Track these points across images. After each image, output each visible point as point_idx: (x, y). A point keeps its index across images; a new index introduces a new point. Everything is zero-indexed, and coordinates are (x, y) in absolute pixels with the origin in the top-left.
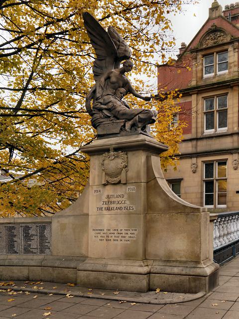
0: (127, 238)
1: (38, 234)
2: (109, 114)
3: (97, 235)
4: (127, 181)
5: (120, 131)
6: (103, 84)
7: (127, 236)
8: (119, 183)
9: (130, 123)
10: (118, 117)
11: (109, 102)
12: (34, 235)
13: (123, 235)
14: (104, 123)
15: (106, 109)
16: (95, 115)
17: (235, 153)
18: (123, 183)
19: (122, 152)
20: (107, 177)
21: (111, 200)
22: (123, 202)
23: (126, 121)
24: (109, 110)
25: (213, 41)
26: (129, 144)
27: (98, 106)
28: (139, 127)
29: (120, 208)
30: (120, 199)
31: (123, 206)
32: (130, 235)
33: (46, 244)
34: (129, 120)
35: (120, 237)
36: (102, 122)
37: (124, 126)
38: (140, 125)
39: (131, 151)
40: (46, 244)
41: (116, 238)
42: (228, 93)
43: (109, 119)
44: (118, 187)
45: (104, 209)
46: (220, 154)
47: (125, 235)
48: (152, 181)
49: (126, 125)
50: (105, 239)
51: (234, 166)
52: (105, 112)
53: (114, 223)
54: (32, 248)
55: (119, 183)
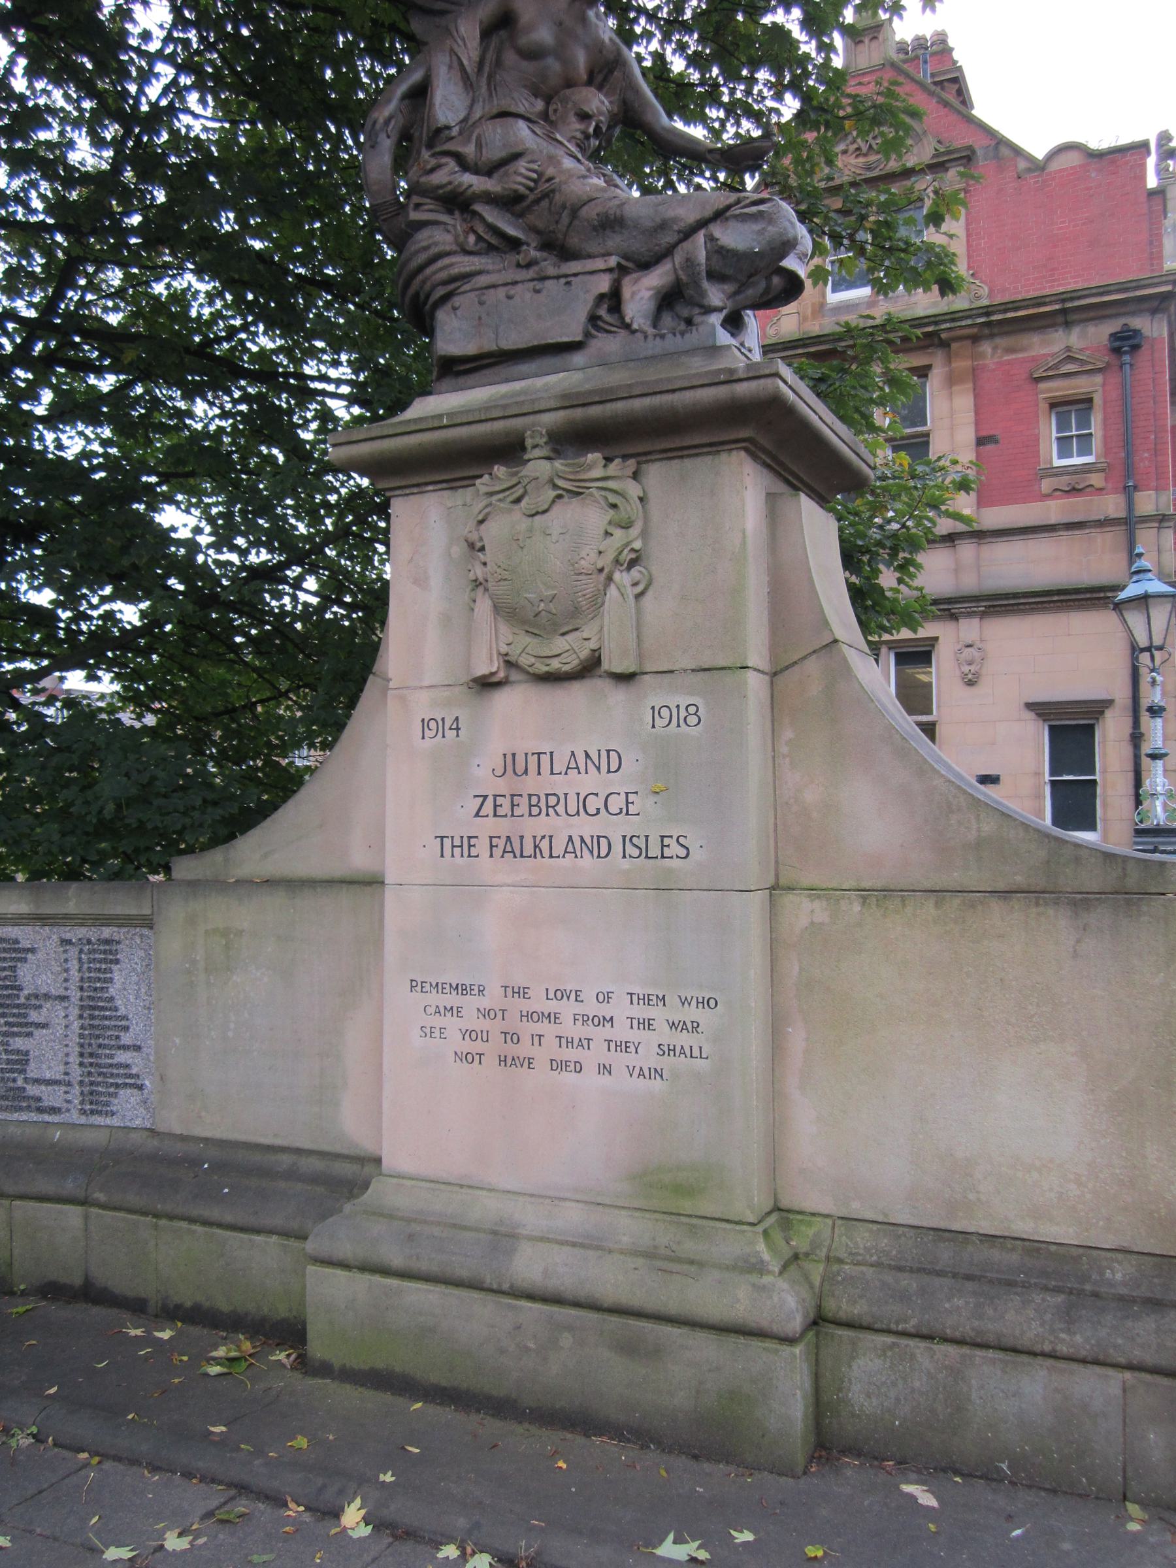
0: (648, 1058)
1: (75, 994)
2: (516, 227)
3: (438, 1022)
4: (640, 656)
5: (587, 335)
6: (475, 55)
7: (649, 1040)
8: (590, 667)
9: (656, 279)
10: (574, 241)
11: (516, 156)
12: (47, 996)
13: (620, 1031)
14: (482, 280)
15: (490, 199)
16: (423, 237)
17: (970, 615)
18: (618, 669)
19: (608, 460)
20: (505, 631)
21: (531, 784)
22: (616, 803)
23: (622, 270)
24: (511, 202)
25: (861, 160)
26: (638, 404)
27: (439, 178)
28: (709, 310)
29: (596, 846)
30: (589, 782)
31: (616, 829)
32: (663, 1034)
33: (122, 1057)
34: (645, 265)
35: (598, 1046)
36: (466, 277)
37: (614, 300)
38: (715, 295)
39: (670, 454)
40: (122, 1057)
41: (571, 1054)
42: (929, 367)
43: (512, 258)
44: (577, 694)
45: (482, 847)
47: (634, 1035)
48: (813, 667)
49: (626, 292)
50: (493, 1048)
51: (966, 669)
52: (491, 215)
54: (37, 1081)
55: (590, 667)
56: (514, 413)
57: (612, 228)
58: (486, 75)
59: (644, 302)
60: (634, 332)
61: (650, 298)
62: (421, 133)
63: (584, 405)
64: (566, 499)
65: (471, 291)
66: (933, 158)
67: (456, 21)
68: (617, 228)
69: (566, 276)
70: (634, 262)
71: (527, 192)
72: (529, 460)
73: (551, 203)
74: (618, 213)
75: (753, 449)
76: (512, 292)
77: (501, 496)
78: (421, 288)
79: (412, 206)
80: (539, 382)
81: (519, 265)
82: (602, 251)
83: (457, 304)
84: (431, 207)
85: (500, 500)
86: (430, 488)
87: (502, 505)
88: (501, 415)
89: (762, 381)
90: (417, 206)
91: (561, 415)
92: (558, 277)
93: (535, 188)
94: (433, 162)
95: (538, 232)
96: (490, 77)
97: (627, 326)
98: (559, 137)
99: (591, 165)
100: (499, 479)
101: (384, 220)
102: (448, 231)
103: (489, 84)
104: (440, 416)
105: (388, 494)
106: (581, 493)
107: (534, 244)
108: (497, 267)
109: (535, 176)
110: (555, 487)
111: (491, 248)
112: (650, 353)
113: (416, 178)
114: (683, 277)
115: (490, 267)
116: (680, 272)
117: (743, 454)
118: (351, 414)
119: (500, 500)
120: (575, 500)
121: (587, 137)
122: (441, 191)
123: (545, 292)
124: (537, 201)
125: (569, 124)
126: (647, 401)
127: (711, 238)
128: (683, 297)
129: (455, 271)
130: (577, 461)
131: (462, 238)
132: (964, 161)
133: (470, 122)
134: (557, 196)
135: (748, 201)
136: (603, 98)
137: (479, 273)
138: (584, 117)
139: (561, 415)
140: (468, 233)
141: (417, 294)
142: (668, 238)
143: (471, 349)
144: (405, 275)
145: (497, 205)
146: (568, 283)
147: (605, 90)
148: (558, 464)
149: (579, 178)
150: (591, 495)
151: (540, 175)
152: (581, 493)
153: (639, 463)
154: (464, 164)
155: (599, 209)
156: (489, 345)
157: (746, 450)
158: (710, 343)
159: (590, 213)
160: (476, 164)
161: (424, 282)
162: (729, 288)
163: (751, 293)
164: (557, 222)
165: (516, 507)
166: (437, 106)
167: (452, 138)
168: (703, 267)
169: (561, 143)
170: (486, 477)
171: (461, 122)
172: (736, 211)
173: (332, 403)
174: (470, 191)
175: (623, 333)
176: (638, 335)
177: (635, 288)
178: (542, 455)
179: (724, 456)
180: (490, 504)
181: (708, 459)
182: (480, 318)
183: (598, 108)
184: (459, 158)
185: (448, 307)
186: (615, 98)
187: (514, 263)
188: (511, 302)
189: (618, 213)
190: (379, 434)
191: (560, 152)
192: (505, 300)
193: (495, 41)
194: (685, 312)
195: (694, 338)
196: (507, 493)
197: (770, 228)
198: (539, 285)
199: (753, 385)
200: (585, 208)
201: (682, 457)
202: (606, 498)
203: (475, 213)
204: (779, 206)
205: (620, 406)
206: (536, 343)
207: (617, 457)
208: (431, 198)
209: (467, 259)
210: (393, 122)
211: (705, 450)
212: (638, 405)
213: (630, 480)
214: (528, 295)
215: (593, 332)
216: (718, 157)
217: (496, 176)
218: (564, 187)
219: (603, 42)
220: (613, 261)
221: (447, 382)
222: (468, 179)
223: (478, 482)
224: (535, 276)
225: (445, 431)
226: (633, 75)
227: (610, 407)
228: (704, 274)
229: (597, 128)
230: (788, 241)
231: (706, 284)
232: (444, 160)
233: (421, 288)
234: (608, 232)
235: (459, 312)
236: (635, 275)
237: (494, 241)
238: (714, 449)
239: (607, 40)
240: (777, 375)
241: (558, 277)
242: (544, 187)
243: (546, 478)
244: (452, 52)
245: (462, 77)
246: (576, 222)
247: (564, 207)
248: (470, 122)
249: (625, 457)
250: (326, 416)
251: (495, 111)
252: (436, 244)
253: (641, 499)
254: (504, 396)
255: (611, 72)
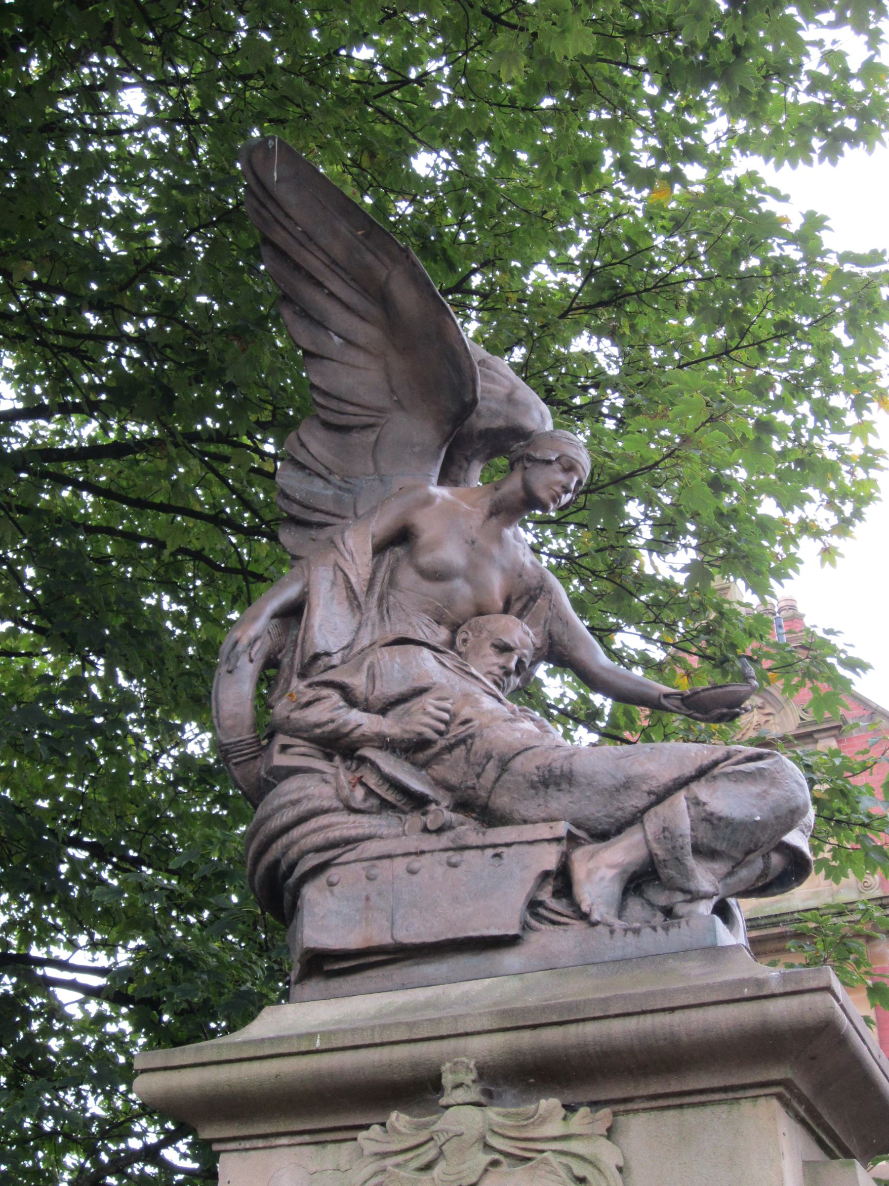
2: (421, 780)
5: (526, 926)
10: (502, 801)
11: (420, 692)
14: (372, 848)
16: (290, 788)
19: (570, 1108)
23: (572, 840)
27: (314, 715)
28: (695, 897)
34: (602, 836)
43: (414, 820)
46: (828, 1146)
53: (38, 1022)
56: (426, 1035)
57: (558, 785)
58: (376, 596)
59: (605, 883)
60: (594, 924)
61: (612, 879)
62: (293, 659)
63: (534, 1027)
64: (504, 1168)
65: (355, 861)
66: (799, 727)
67: (343, 533)
68: (564, 786)
69: (495, 846)
70: (587, 830)
71: (435, 736)
72: (447, 1107)
73: (469, 751)
74: (566, 768)
75: (788, 1096)
76: (416, 865)
77: (400, 1158)
78: (284, 854)
79: (277, 748)
80: (455, 991)
81: (425, 830)
82: (543, 815)
83: (334, 879)
84: (303, 750)
85: (398, 1165)
86: (284, 1141)
87: (402, 1173)
88: (405, 1037)
89: (806, 998)
90: (284, 748)
91: (499, 1041)
92: (483, 847)
93: (447, 732)
94: (310, 694)
95: (449, 788)
96: (381, 599)
97: (584, 917)
98: (474, 671)
99: (515, 706)
100: (398, 1132)
101: (236, 764)
102: (326, 782)
103: (380, 605)
104: (311, 1036)
105: (216, 1147)
106: (529, 1159)
107: (445, 803)
108: (393, 831)
109: (446, 716)
110: (488, 1147)
111: (385, 805)
112: (619, 954)
113: (286, 714)
114: (660, 853)
115: (385, 831)
116: (654, 846)
117: (775, 1103)
118: (86, 1013)
119: (398, 1165)
120: (520, 1169)
121: (507, 673)
122: (318, 731)
123: (463, 867)
124: (450, 748)
125: (484, 656)
126: (632, 1024)
127: (696, 802)
128: (658, 878)
129: (335, 834)
130: (521, 1109)
131: (346, 792)
132: (835, 732)
133: (357, 648)
134: (478, 742)
135: (741, 756)
136: (527, 628)
137: (369, 838)
138: (504, 649)
139: (499, 1041)
140: (354, 786)
141: (277, 863)
142: (638, 801)
143: (352, 940)
144: (260, 837)
145: (394, 751)
146: (497, 855)
147: (526, 619)
148: (493, 1114)
149: (505, 721)
150: (546, 1162)
151: (454, 716)
152: (529, 1159)
153: (615, 1114)
154: (351, 701)
155: (539, 761)
156: (381, 937)
157: (779, 1097)
158: (708, 942)
159: (523, 765)
160: (366, 700)
161: (288, 847)
162: (721, 867)
163: (747, 874)
164: (478, 776)
165: (425, 1177)
166: (316, 628)
167: (333, 667)
168: (688, 840)
169: (477, 678)
170: (376, 1128)
171: (344, 648)
172: (727, 768)
173: (63, 995)
174: (358, 733)
175: (578, 926)
176: (600, 928)
177: (591, 865)
178: (468, 1099)
179: (746, 1107)
180: (384, 1171)
181: (721, 1111)
182: (367, 899)
183: (520, 640)
184: (343, 690)
185: (322, 880)
186: (540, 629)
187: (420, 825)
188: (415, 878)
189: (566, 768)
190: (215, 1058)
191: (475, 689)
192: (405, 875)
193: (388, 558)
194: (662, 899)
195: (680, 935)
196: (410, 1155)
197: (773, 791)
198: (455, 857)
199: (794, 1003)
200: (520, 759)
201: (681, 1106)
202: (569, 1169)
203: (363, 760)
204: (783, 763)
205: (590, 1030)
206: (450, 936)
207: (581, 1104)
208: (304, 739)
209: (353, 817)
210: (258, 644)
211: (717, 1097)
212: (619, 1029)
213: (604, 1141)
214: (440, 870)
215: (533, 922)
216: (678, 703)
217: (391, 714)
218: (486, 732)
219: (523, 565)
220: (562, 828)
221: (314, 985)
222: (356, 716)
223: (362, 1135)
224: (451, 845)
225: (316, 1057)
226: (561, 603)
227: (573, 1030)
228: (689, 848)
229: (520, 662)
230: (798, 808)
231: (691, 861)
232: (325, 692)
233: (284, 854)
234: (552, 790)
235: (336, 889)
236: (590, 848)
237: (390, 797)
238: (731, 1095)
239: (528, 564)
240: (828, 989)
241: (483, 847)
242: (457, 731)
243: (476, 1134)
244: (337, 567)
245: (348, 597)
246: (506, 777)
247: (489, 757)
248: (357, 648)
249: (595, 1105)
250: (54, 1011)
251: (391, 637)
252: (309, 798)
253: (620, 1169)
254: (399, 1010)
255: (533, 599)
